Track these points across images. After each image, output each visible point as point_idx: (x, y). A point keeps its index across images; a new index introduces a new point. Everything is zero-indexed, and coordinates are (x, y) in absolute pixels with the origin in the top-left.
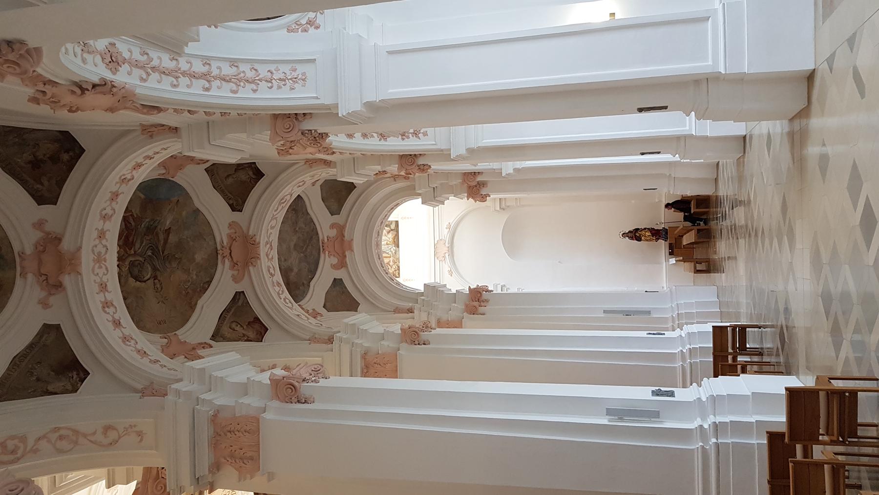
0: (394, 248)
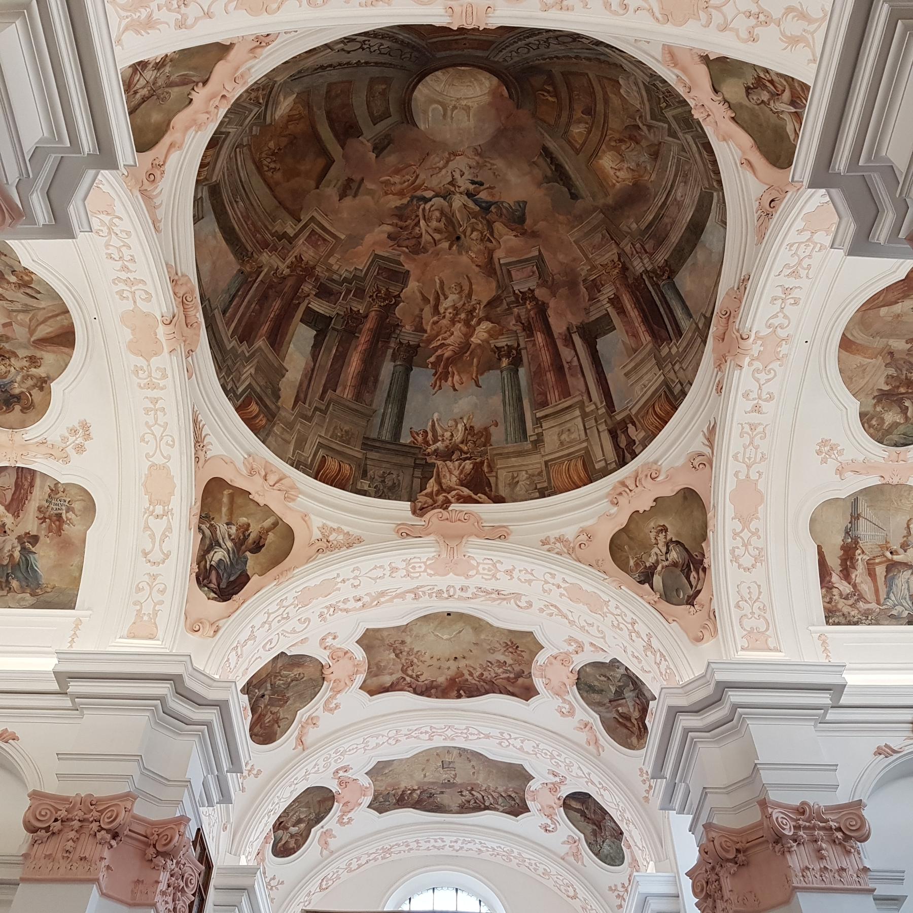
0: (905, 614)
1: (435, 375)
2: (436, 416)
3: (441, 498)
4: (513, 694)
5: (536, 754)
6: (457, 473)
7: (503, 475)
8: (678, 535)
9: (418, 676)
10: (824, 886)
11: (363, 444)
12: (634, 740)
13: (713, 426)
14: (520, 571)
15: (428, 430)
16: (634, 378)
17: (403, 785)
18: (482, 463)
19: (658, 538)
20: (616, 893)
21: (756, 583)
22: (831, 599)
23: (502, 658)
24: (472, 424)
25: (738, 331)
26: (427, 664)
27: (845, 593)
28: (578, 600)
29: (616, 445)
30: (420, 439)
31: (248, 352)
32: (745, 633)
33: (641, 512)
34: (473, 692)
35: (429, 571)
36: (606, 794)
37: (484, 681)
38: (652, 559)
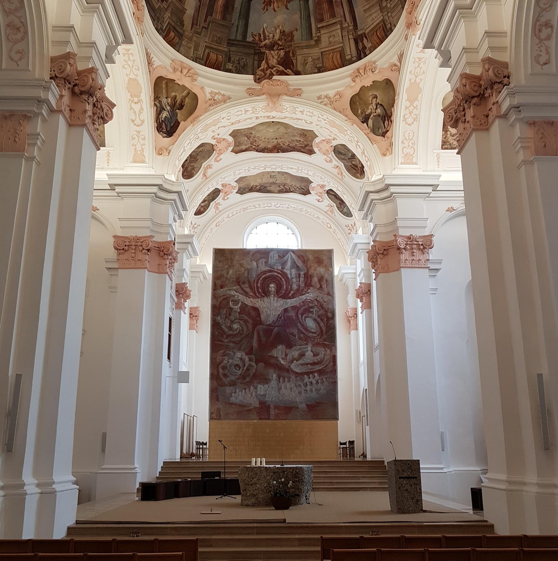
1: (264, 3)
3: (268, 72)
4: (304, 152)
5: (314, 176)
6: (276, 57)
8: (382, 101)
9: (258, 145)
10: (412, 266)
11: (228, 43)
12: (359, 175)
13: (402, 54)
14: (307, 112)
15: (261, 33)
16: (368, 13)
17: (252, 184)
18: (289, 51)
19: (373, 101)
20: (348, 228)
21: (412, 131)
22: (446, 136)
23: (299, 139)
24: (284, 30)
25: (416, 18)
26: (262, 141)
27: (453, 134)
28: (334, 127)
30: (257, 38)
31: (166, 5)
32: (404, 155)
33: (366, 86)
34: (284, 151)
35: (263, 111)
36: (344, 196)
37: (290, 147)
38: (369, 111)
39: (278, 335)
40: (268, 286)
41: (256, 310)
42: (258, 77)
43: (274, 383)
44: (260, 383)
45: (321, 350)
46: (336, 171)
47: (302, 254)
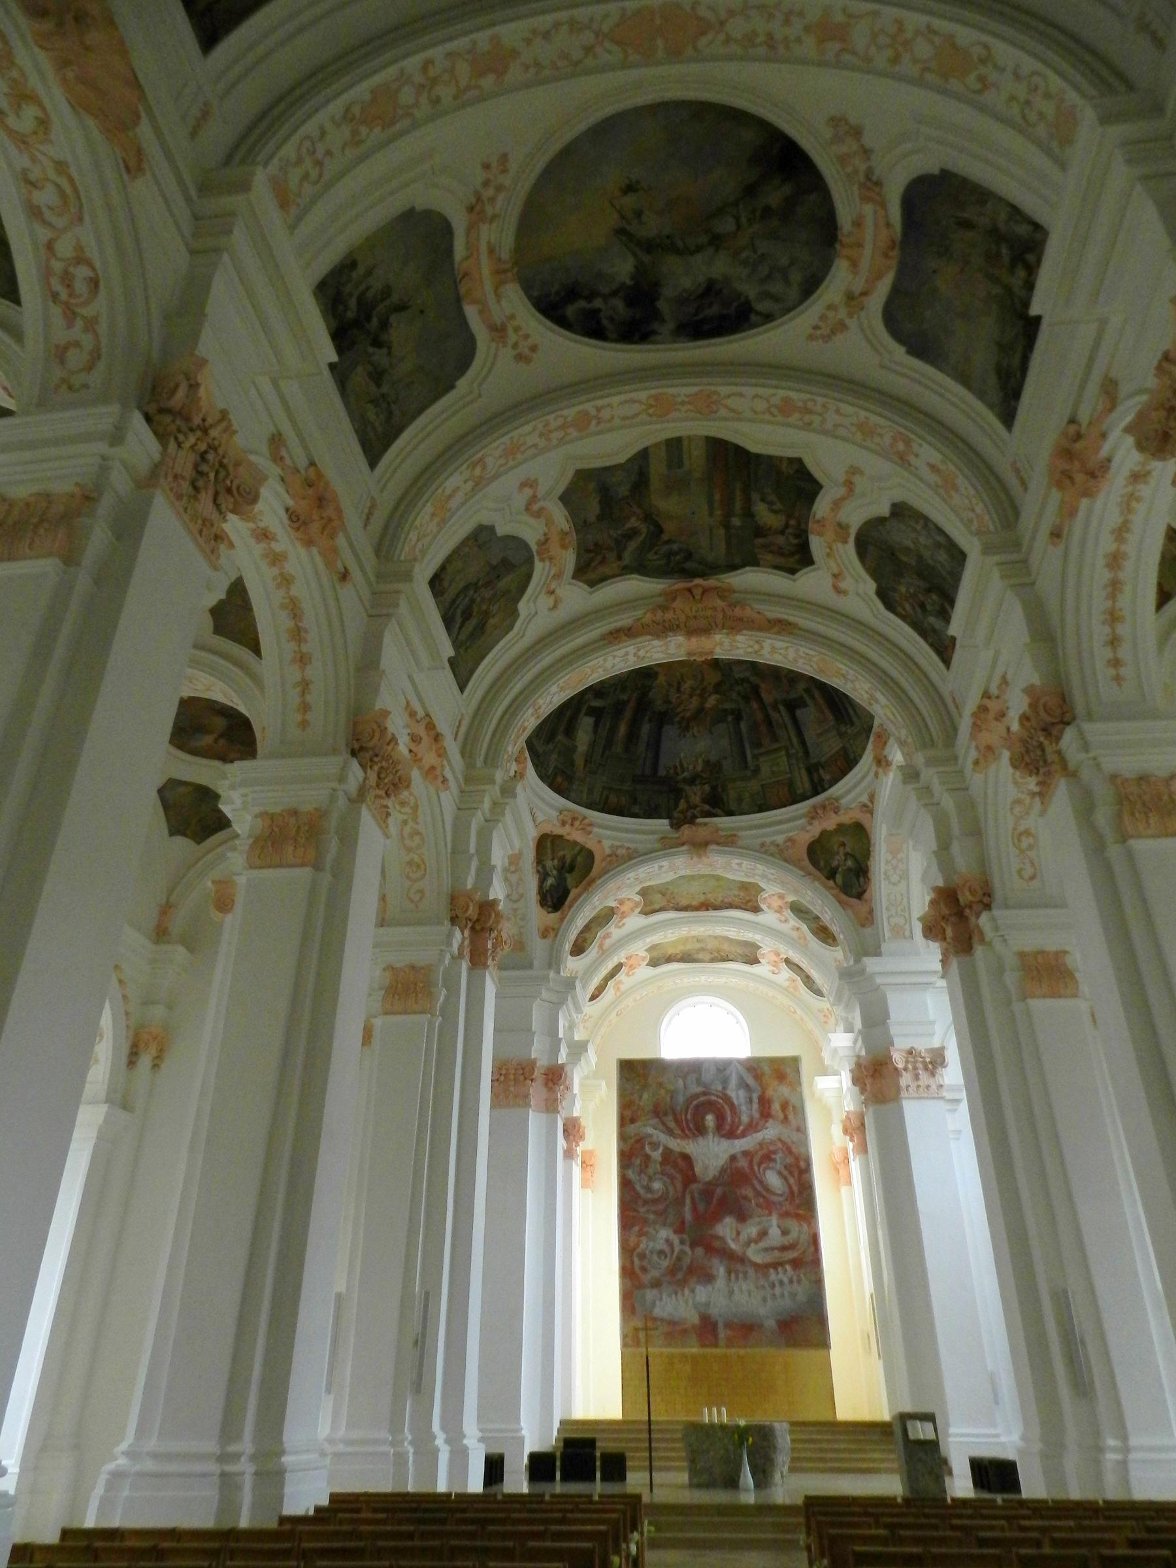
2: (682, 755)
6: (699, 793)
7: (732, 794)
29: (812, 780)
39: (723, 1201)
40: (703, 1119)
41: (687, 1158)
42: (675, 821)
43: (721, 1282)
44: (698, 1282)
45: (792, 1224)
46: (795, 934)
47: (754, 1067)
